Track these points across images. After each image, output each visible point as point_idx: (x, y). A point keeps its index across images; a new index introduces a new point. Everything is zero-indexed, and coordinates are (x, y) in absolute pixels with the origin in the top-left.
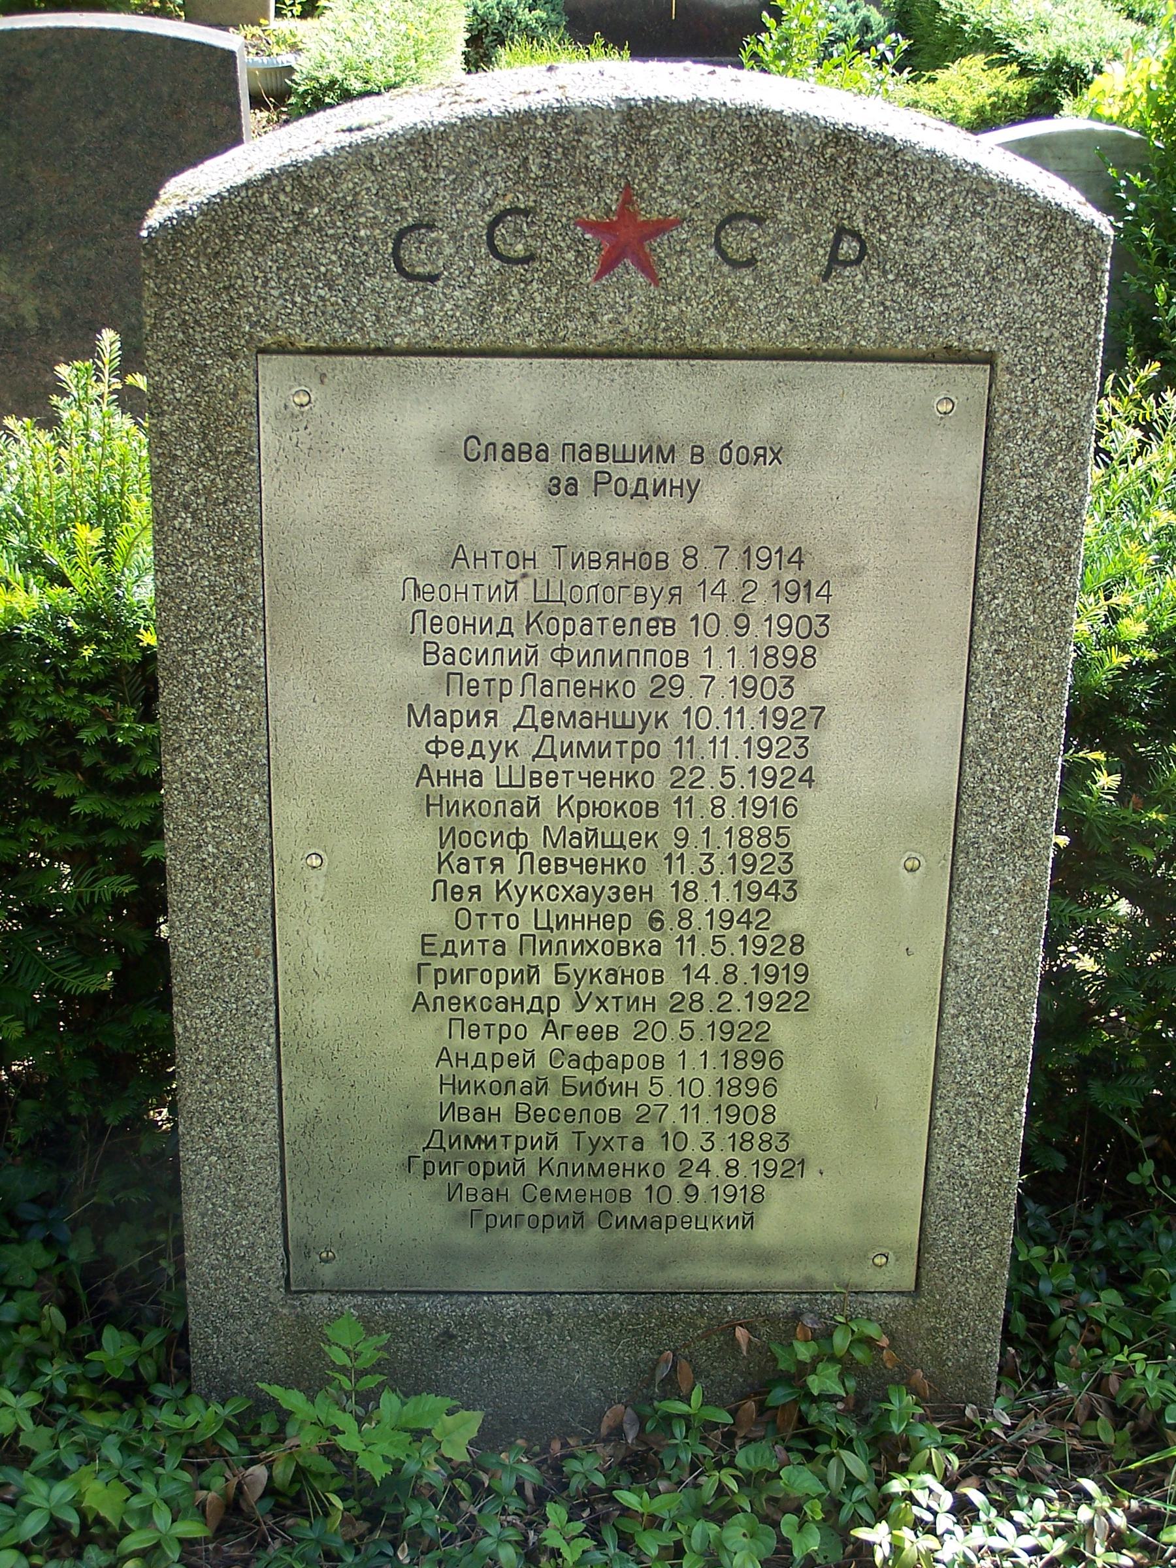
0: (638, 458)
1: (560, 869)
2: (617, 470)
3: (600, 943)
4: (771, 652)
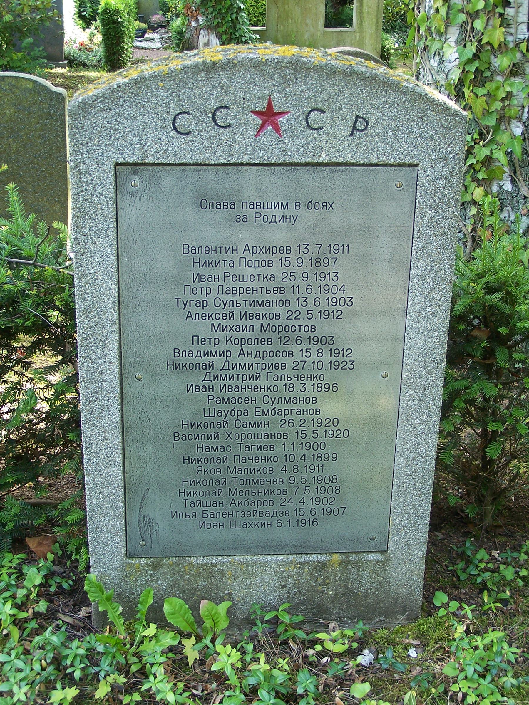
0: (273, 207)
1: (313, 330)
2: (263, 212)
3: (258, 252)
4: (319, 455)
